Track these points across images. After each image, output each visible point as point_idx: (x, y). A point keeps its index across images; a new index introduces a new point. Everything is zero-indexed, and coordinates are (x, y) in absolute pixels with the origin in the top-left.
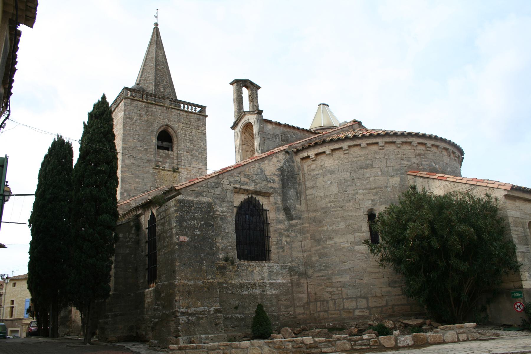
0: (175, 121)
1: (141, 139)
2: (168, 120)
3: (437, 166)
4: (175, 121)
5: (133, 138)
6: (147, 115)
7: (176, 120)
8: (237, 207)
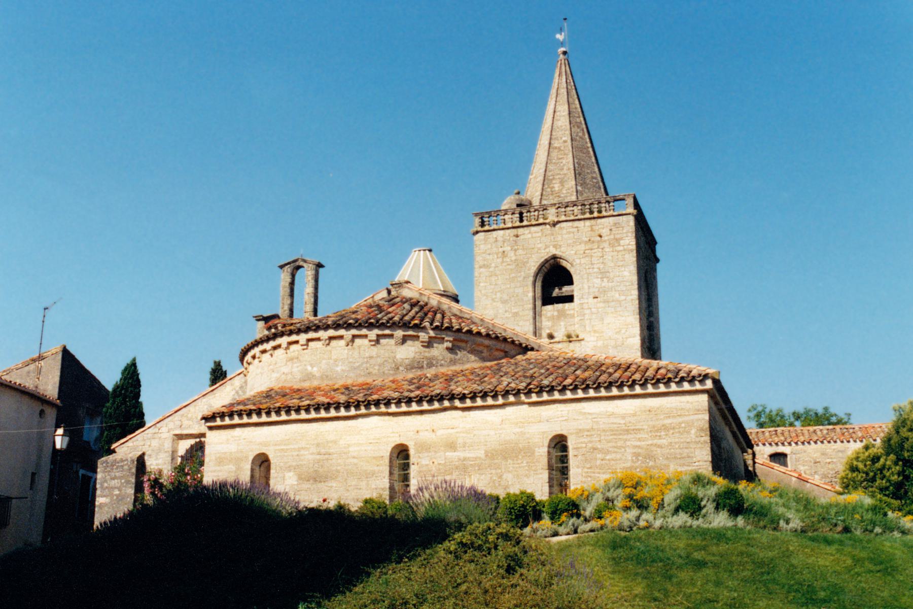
0: (568, 245)
1: (505, 297)
2: (555, 246)
3: (315, 369)
4: (568, 245)
5: (493, 300)
6: (516, 250)
7: (571, 241)
8: (182, 457)
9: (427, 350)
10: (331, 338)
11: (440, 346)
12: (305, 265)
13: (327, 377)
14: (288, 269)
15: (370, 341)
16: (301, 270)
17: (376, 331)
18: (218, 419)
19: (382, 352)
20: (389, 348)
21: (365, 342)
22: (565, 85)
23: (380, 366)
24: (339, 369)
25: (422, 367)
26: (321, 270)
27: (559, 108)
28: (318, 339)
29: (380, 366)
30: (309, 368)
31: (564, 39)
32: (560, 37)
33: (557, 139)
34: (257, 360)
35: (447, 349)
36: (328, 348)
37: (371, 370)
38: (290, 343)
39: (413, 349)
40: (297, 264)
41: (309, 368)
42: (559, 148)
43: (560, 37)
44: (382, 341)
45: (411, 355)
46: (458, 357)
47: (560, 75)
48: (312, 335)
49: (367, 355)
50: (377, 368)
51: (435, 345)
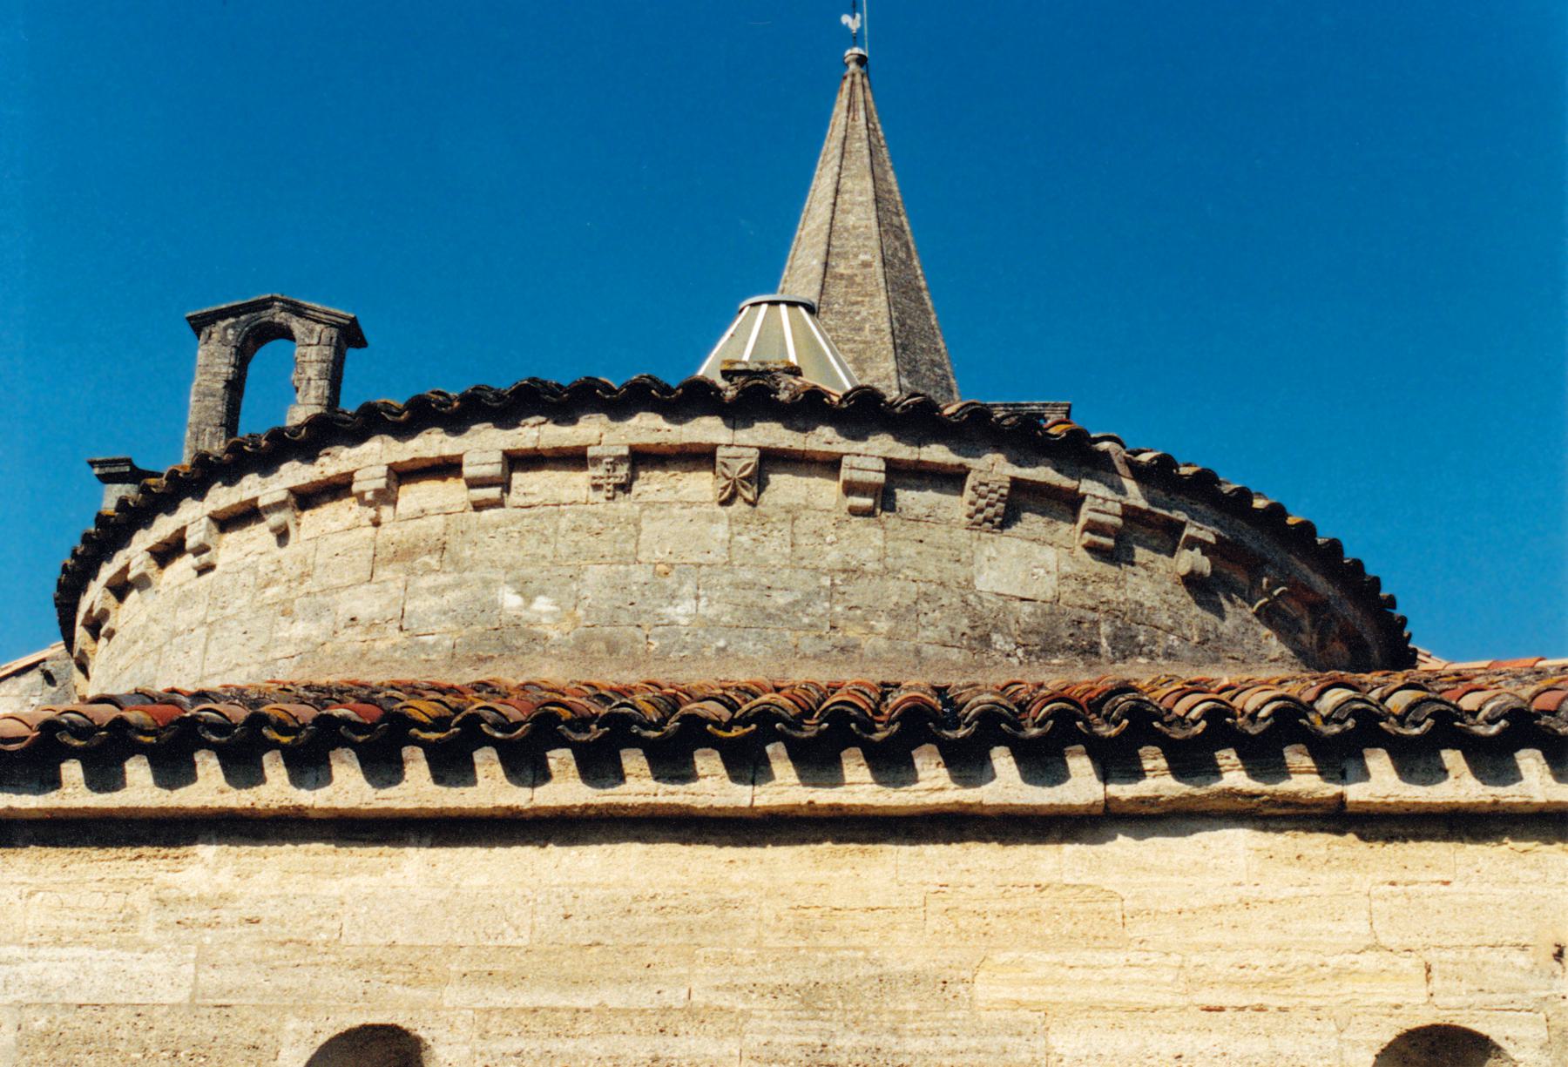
3: (542, 604)
9: (1110, 570)
10: (643, 458)
11: (1162, 562)
12: (297, 325)
13: (612, 648)
14: (222, 338)
15: (850, 489)
16: (280, 344)
17: (883, 446)
18: (72, 771)
19: (910, 550)
20: (939, 534)
21: (826, 491)
22: (864, 133)
23: (896, 615)
24: (681, 611)
25: (1093, 650)
26: (352, 354)
27: (847, 184)
28: (575, 459)
29: (896, 615)
30: (510, 600)
31: (860, 30)
32: (851, 22)
33: (843, 256)
34: (184, 565)
35: (1192, 581)
36: (624, 504)
37: (854, 632)
38: (403, 474)
39: (1050, 555)
40: (265, 316)
41: (510, 600)
42: (851, 278)
43: (851, 22)
44: (905, 497)
45: (1045, 588)
46: (1226, 627)
47: (851, 107)
48: (535, 433)
49: (833, 556)
50: (883, 625)
51: (1141, 554)
